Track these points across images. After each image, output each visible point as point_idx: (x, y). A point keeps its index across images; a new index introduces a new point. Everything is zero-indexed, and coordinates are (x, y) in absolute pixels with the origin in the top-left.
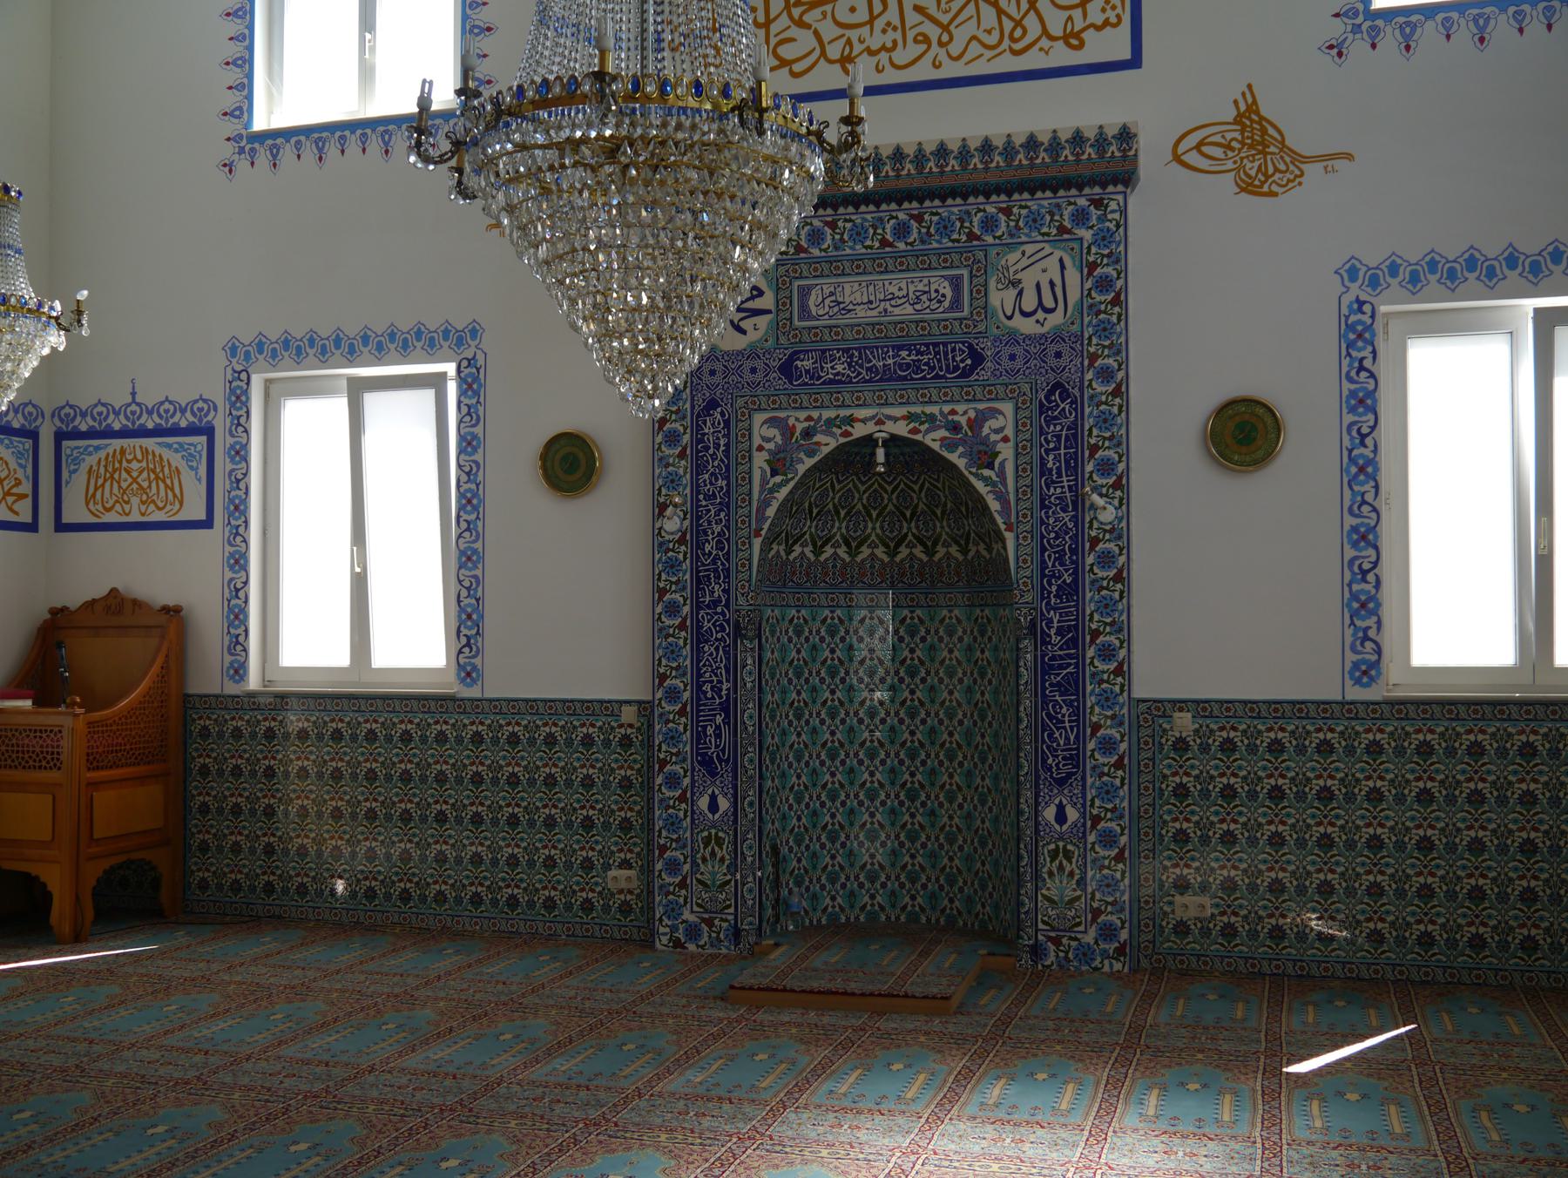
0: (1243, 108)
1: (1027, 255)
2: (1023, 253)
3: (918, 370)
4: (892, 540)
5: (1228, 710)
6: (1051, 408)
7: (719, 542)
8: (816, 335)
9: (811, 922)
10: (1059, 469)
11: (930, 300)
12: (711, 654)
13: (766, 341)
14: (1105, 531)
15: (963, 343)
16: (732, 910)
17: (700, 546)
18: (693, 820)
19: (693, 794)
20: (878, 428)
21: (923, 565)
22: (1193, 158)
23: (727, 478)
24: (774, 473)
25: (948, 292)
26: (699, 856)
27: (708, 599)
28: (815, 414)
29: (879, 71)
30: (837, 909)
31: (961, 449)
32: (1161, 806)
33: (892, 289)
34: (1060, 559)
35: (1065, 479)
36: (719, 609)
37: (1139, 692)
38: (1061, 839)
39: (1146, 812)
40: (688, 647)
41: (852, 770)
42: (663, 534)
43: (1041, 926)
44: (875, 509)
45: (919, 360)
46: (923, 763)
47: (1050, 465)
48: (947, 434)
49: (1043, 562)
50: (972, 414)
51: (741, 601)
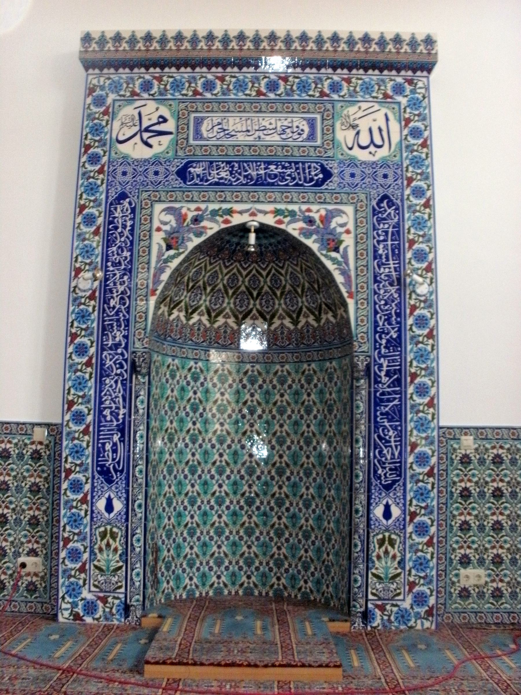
2: (360, 108)
3: (283, 179)
7: (122, 299)
12: (111, 386)
15: (317, 163)
16: (123, 590)
17: (106, 301)
18: (92, 518)
19: (93, 497)
20: (252, 218)
23: (131, 250)
24: (169, 247)
25: (307, 129)
26: (96, 547)
27: (110, 343)
28: (203, 206)
31: (314, 237)
33: (265, 123)
34: (388, 320)
35: (391, 262)
36: (119, 351)
45: (283, 173)
48: (304, 225)
49: (376, 322)
50: (323, 213)
51: (138, 345)
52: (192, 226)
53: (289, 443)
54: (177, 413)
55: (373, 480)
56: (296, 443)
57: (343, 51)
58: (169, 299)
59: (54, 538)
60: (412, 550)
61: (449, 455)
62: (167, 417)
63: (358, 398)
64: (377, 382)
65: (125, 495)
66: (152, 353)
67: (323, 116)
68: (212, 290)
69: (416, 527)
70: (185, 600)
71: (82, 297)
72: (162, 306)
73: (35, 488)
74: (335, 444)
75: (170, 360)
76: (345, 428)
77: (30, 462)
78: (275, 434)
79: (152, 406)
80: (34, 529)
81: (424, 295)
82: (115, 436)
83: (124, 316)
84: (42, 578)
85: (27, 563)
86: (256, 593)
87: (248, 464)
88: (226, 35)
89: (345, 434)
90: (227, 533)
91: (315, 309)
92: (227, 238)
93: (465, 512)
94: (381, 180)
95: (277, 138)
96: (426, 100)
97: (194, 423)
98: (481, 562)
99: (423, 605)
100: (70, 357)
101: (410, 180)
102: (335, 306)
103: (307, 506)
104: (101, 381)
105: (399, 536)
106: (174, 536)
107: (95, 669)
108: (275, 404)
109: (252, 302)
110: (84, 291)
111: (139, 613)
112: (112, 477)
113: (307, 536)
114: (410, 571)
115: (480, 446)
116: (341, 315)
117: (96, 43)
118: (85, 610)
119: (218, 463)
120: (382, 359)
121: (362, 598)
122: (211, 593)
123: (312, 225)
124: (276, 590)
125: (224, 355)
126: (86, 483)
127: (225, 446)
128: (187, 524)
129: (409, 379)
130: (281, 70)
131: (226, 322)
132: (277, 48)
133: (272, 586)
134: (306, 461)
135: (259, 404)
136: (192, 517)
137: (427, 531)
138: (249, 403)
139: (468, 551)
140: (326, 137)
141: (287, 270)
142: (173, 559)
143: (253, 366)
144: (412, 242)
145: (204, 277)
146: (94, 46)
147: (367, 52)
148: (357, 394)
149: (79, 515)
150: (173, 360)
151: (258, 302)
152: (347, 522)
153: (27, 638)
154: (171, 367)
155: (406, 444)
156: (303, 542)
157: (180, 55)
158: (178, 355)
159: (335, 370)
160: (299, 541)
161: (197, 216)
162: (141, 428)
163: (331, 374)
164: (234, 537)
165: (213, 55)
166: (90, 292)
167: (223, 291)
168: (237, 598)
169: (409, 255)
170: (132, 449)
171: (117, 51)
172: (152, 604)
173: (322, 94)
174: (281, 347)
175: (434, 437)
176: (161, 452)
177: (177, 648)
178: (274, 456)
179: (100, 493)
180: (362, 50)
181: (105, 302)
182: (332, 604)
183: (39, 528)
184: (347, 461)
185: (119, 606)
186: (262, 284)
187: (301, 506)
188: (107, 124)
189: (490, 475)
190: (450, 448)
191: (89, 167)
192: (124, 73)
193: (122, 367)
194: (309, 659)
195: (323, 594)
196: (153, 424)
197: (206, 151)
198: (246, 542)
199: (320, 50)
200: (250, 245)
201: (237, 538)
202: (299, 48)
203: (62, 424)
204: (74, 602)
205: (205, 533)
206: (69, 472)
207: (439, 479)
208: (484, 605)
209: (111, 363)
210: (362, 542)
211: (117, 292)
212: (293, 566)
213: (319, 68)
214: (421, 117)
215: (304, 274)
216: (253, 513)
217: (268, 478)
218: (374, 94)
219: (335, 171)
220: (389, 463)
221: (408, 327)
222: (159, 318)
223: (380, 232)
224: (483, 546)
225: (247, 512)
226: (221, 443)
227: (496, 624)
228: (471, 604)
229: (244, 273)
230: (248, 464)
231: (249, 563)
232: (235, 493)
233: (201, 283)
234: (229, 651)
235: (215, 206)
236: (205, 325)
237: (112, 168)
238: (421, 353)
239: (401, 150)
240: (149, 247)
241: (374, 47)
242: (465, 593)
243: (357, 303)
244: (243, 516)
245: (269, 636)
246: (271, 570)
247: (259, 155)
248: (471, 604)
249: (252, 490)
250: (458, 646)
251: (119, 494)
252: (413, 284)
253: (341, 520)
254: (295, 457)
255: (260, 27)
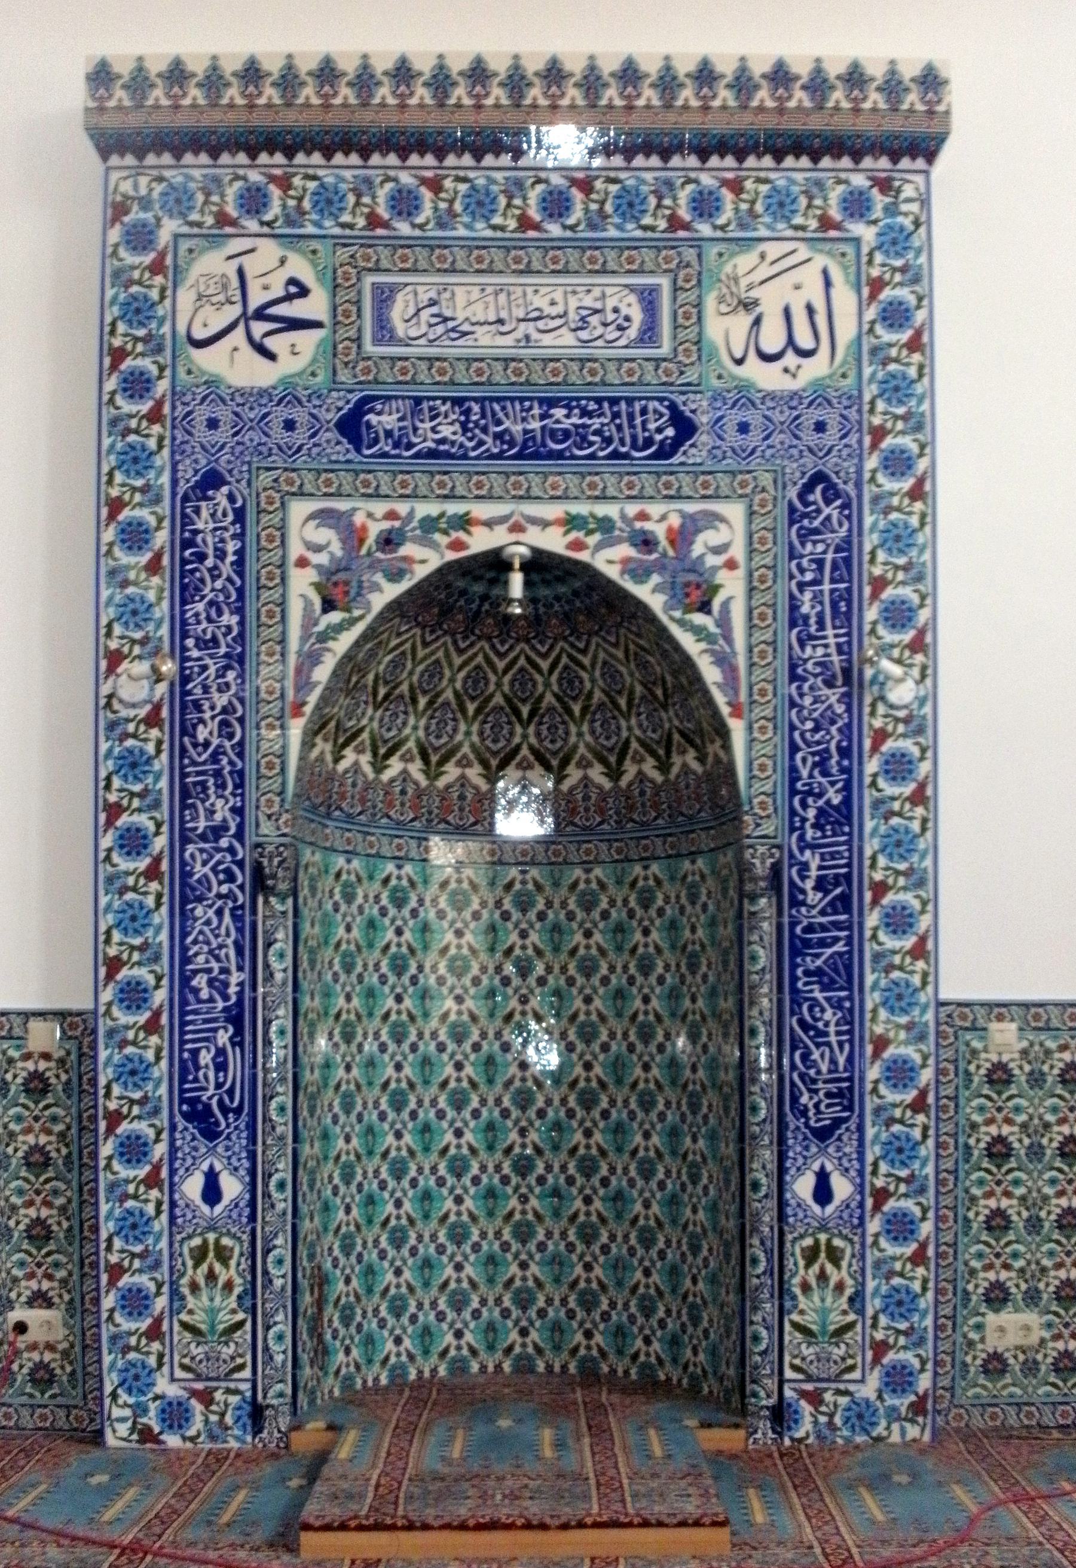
2: (763, 256)
3: (583, 442)
7: (225, 724)
12: (208, 923)
15: (661, 400)
16: (247, 1373)
17: (187, 730)
19: (173, 1172)
20: (514, 537)
23: (240, 611)
24: (328, 605)
25: (637, 315)
26: (184, 1281)
27: (202, 824)
28: (402, 508)
31: (655, 579)
33: (540, 302)
36: (224, 843)
45: (584, 426)
49: (793, 769)
50: (675, 521)
51: (266, 828)
52: (380, 555)
53: (604, 1037)
54: (360, 977)
55: (790, 1117)
56: (619, 1036)
57: (724, 107)
58: (333, 724)
59: (87, 1266)
60: (879, 1273)
61: (962, 1065)
62: (338, 988)
63: (755, 938)
64: (795, 903)
65: (246, 1164)
66: (300, 846)
67: (675, 281)
68: (431, 703)
69: (888, 1222)
70: (386, 1388)
71: (128, 720)
72: (318, 740)
73: (36, 1157)
74: (704, 1039)
75: (340, 861)
76: (727, 1004)
77: (22, 1101)
78: (573, 1018)
79: (305, 964)
80: (39, 1249)
81: (906, 707)
82: (221, 1032)
84: (65, 1354)
85: (29, 1323)
86: (541, 1367)
87: (517, 1083)
88: (441, 67)
89: (726, 1017)
90: (475, 1237)
91: (658, 743)
92: (461, 584)
93: (999, 1190)
94: (810, 437)
95: (567, 338)
96: (922, 230)
97: (399, 999)
98: (1032, 1298)
99: (904, 1391)
100: (108, 859)
101: (879, 434)
102: (702, 737)
103: (647, 1174)
104: (183, 912)
105: (851, 1241)
106: (359, 1248)
107: (192, 1544)
108: (573, 952)
109: (519, 730)
110: (134, 706)
111: (284, 1422)
112: (217, 1123)
113: (647, 1241)
114: (875, 1318)
115: (1032, 1044)
116: (716, 755)
117: (125, 87)
118: (164, 1420)
119: (452, 1084)
120: (808, 853)
121: (770, 1376)
122: (442, 1371)
123: (650, 552)
124: (584, 1360)
125: (460, 849)
126: (157, 1140)
127: (467, 1046)
128: (387, 1220)
129: (868, 896)
130: (575, 162)
131: (463, 776)
132: (565, 102)
133: (574, 1351)
134: (643, 1075)
135: (539, 953)
136: (398, 1204)
137: (912, 1232)
138: (517, 951)
139: (1004, 1275)
140: (682, 335)
141: (595, 657)
142: (358, 1298)
143: (524, 872)
144: (879, 584)
145: (411, 673)
146: (120, 95)
147: (781, 111)
148: (752, 929)
149: (142, 1214)
150: (349, 861)
151: (531, 730)
152: (734, 1208)
153: (39, 1483)
154: (344, 877)
155: (862, 1038)
156: (640, 1252)
157: (333, 120)
158: (359, 849)
159: (703, 877)
160: (632, 1251)
161: (390, 531)
162: (281, 1012)
163: (693, 886)
164: (491, 1244)
165: (412, 120)
167: (454, 706)
168: (500, 1379)
169: (871, 614)
170: (260, 1060)
171: (176, 107)
172: (312, 1402)
173: (675, 223)
174: (585, 828)
175: (926, 1024)
176: (327, 1065)
177: (371, 1495)
178: (573, 1066)
179: (189, 1161)
180: (770, 104)
181: (184, 732)
182: (706, 1390)
183: (52, 1246)
184: (731, 1076)
185: (239, 1408)
186: (540, 688)
187: (633, 1173)
188: (162, 297)
189: (1055, 1110)
190: (963, 1048)
191: (127, 407)
192: (197, 166)
193: (231, 878)
194: (659, 1510)
195: (686, 1367)
196: (306, 1002)
197: (404, 371)
198: (516, 1256)
199: (668, 106)
200: (512, 600)
201: (496, 1246)
202: (619, 102)
203: (95, 1012)
204: (138, 1405)
205: (427, 1238)
206: (115, 1118)
207: (938, 1118)
208: (1035, 1388)
209: (207, 869)
210: (768, 1253)
211: (212, 708)
212: (620, 1306)
213: (666, 154)
214: (909, 275)
215: (632, 665)
216: (531, 1190)
217: (562, 1114)
218: (798, 220)
219: (703, 420)
220: (826, 1082)
221: (867, 780)
222: (313, 767)
223: (805, 562)
224: (1038, 1263)
225: (516, 1189)
226: (459, 1039)
227: (1061, 1427)
228: (1009, 1388)
229: (501, 665)
230: (517, 1083)
231: (524, 1301)
232: (491, 1148)
233: (405, 688)
234: (484, 1496)
235: (432, 509)
236: (416, 783)
237: (180, 410)
238: (896, 837)
239: (859, 361)
240: (283, 604)
241: (800, 97)
242: (995, 1366)
243: (750, 728)
244: (508, 1198)
245: (571, 1462)
246: (571, 1315)
247: (528, 383)
248: (1009, 1388)
249: (528, 1141)
250: (979, 1474)
251: (234, 1160)
252: (881, 681)
253: (721, 1204)
254: (618, 1067)
255: (524, 48)
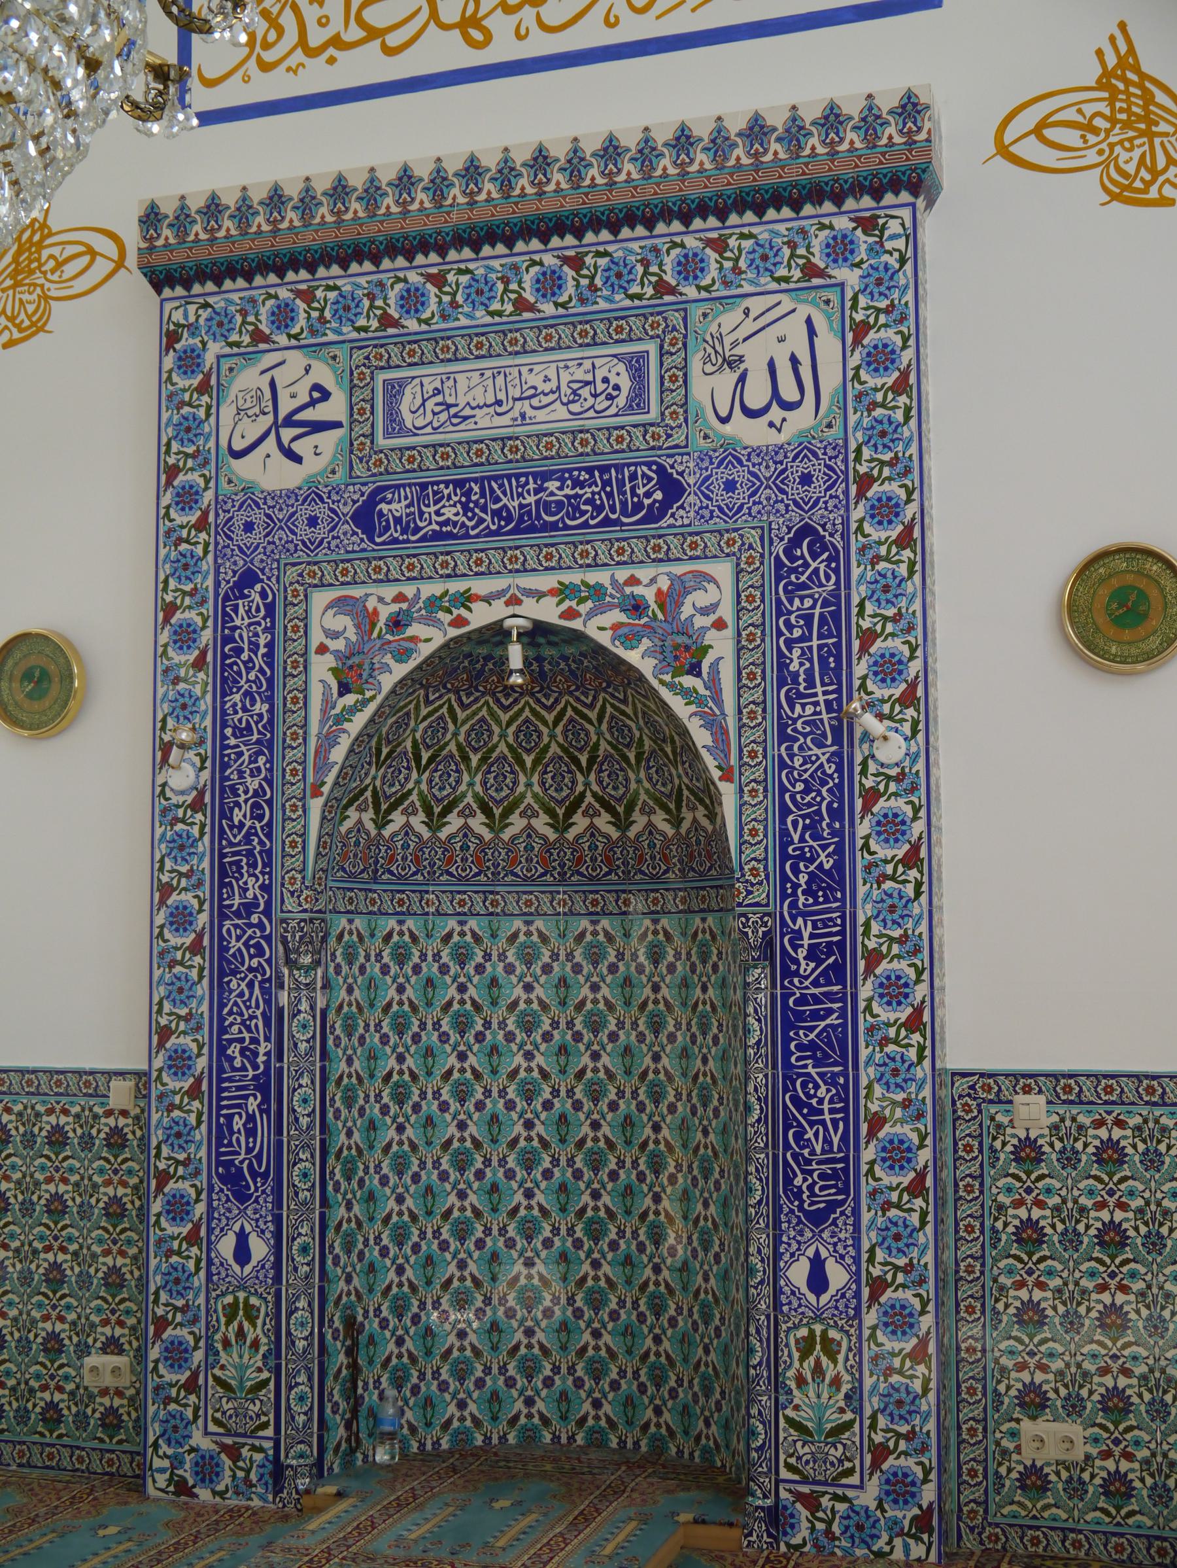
0: (1111, 60)
1: (752, 315)
2: (747, 312)
3: (576, 511)
4: (560, 803)
5: (1109, 1090)
6: (794, 570)
7: (256, 806)
8: (411, 460)
9: (422, 1445)
10: (809, 673)
11: (595, 396)
12: (241, 995)
13: (333, 472)
14: (889, 778)
15: (649, 465)
16: (269, 1432)
17: (226, 814)
18: (209, 1275)
19: (210, 1231)
20: (510, 610)
21: (611, 844)
22: (1030, 149)
23: (270, 700)
24: (344, 689)
25: (625, 383)
26: (218, 1337)
27: (237, 901)
28: (409, 590)
29: (519, 37)
30: (468, 1423)
31: (646, 643)
32: (995, 1260)
33: (535, 380)
34: (813, 827)
35: (819, 689)
36: (254, 919)
37: (955, 1057)
38: (818, 1318)
39: (970, 1270)
40: (205, 982)
41: (494, 1188)
42: (169, 794)
43: (784, 1474)
44: (528, 751)
45: (577, 496)
46: (613, 1176)
47: (794, 667)
48: (622, 618)
49: (784, 833)
50: (664, 584)
51: (290, 903)
52: (389, 637)
82: (251, 1099)
83: (261, 843)
110: (182, 793)
112: (248, 1187)
114: (874, 1417)
166: (195, 793)
181: (223, 815)
200: (511, 672)
209: (240, 944)
211: (246, 792)
220: (819, 1163)
